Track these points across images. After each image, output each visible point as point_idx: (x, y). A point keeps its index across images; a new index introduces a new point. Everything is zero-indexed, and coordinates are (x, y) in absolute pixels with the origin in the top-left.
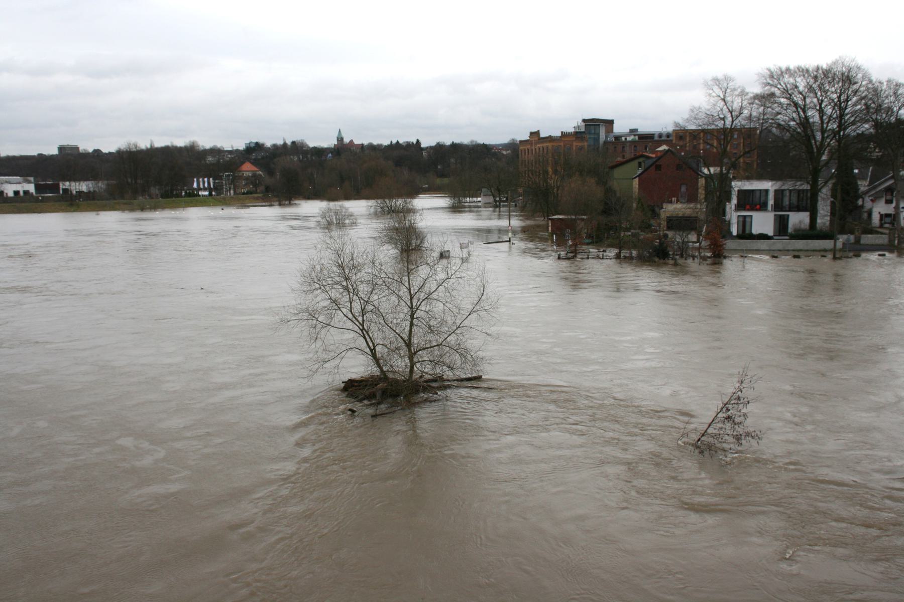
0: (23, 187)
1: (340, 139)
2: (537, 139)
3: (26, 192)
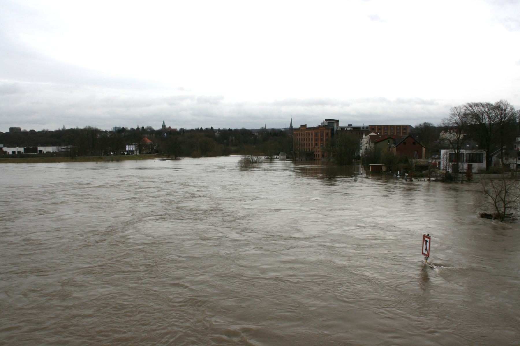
0: (17, 149)
1: (164, 126)
2: (305, 128)
3: (19, 152)
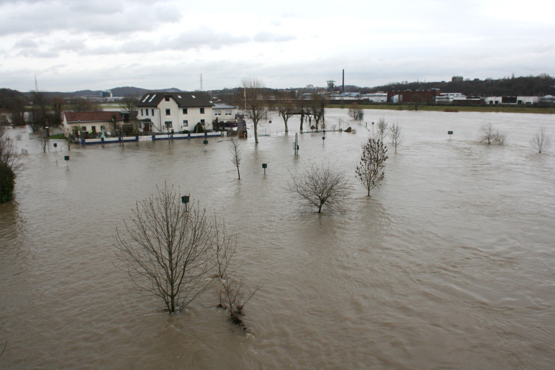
3: (497, 102)
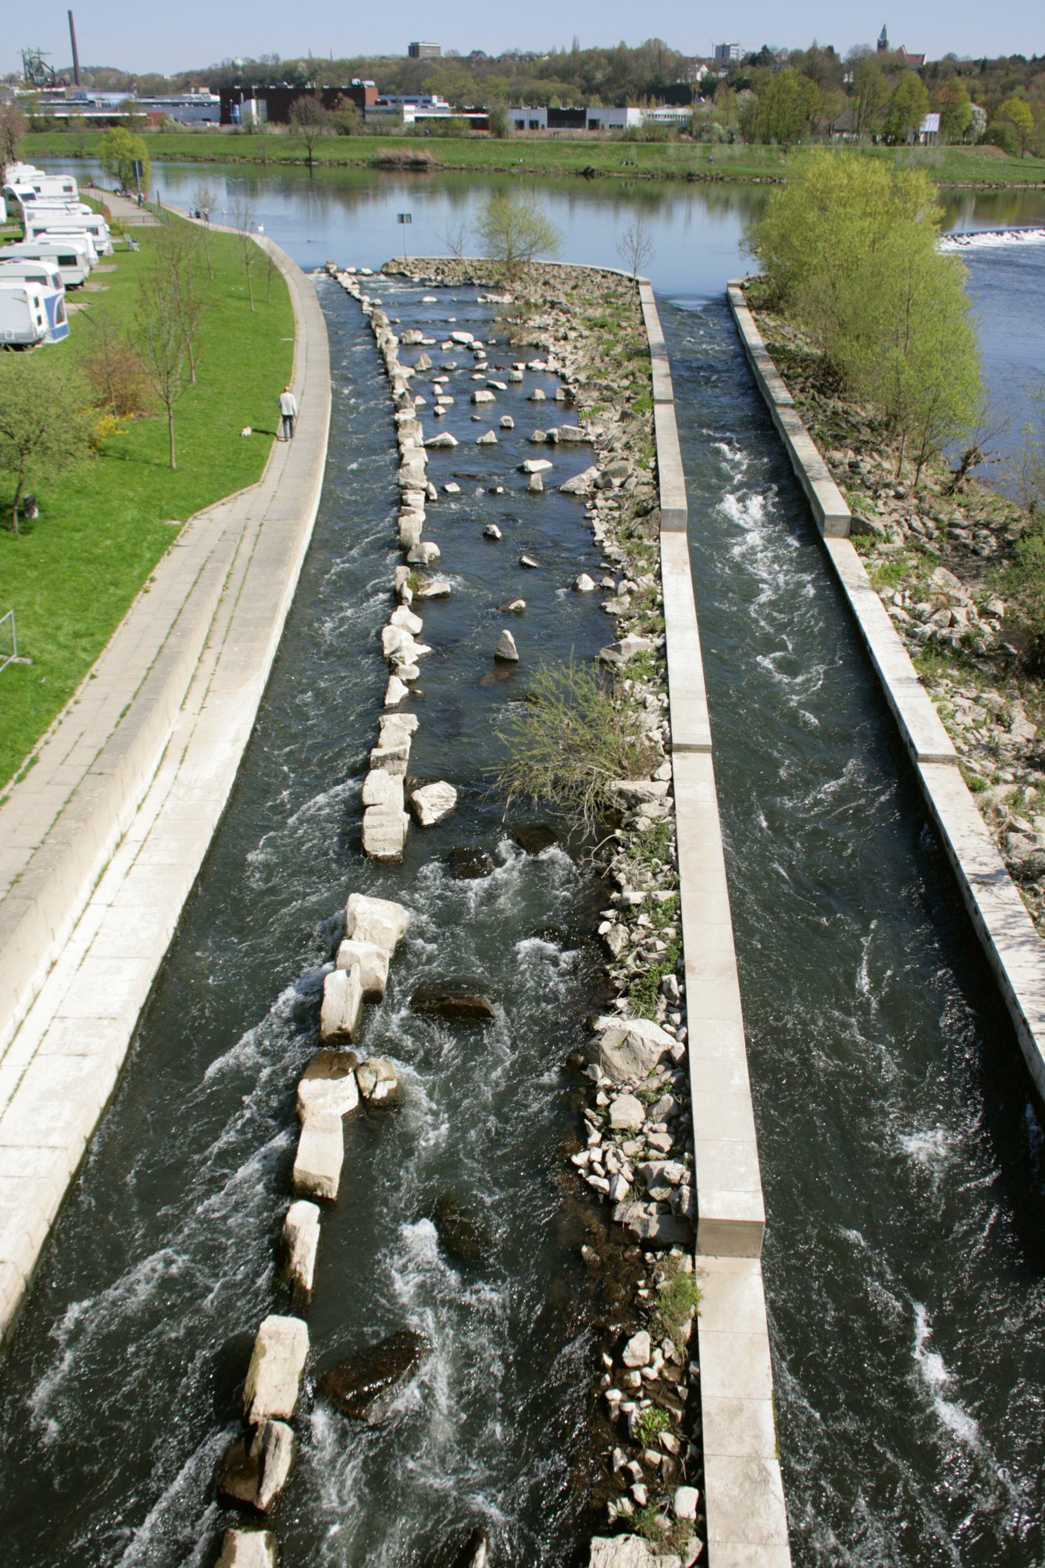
1: (882, 45)
